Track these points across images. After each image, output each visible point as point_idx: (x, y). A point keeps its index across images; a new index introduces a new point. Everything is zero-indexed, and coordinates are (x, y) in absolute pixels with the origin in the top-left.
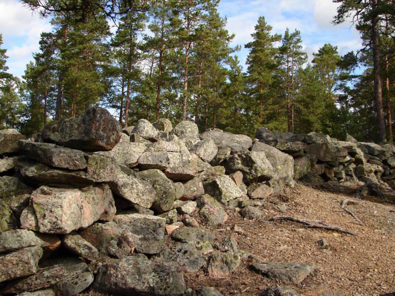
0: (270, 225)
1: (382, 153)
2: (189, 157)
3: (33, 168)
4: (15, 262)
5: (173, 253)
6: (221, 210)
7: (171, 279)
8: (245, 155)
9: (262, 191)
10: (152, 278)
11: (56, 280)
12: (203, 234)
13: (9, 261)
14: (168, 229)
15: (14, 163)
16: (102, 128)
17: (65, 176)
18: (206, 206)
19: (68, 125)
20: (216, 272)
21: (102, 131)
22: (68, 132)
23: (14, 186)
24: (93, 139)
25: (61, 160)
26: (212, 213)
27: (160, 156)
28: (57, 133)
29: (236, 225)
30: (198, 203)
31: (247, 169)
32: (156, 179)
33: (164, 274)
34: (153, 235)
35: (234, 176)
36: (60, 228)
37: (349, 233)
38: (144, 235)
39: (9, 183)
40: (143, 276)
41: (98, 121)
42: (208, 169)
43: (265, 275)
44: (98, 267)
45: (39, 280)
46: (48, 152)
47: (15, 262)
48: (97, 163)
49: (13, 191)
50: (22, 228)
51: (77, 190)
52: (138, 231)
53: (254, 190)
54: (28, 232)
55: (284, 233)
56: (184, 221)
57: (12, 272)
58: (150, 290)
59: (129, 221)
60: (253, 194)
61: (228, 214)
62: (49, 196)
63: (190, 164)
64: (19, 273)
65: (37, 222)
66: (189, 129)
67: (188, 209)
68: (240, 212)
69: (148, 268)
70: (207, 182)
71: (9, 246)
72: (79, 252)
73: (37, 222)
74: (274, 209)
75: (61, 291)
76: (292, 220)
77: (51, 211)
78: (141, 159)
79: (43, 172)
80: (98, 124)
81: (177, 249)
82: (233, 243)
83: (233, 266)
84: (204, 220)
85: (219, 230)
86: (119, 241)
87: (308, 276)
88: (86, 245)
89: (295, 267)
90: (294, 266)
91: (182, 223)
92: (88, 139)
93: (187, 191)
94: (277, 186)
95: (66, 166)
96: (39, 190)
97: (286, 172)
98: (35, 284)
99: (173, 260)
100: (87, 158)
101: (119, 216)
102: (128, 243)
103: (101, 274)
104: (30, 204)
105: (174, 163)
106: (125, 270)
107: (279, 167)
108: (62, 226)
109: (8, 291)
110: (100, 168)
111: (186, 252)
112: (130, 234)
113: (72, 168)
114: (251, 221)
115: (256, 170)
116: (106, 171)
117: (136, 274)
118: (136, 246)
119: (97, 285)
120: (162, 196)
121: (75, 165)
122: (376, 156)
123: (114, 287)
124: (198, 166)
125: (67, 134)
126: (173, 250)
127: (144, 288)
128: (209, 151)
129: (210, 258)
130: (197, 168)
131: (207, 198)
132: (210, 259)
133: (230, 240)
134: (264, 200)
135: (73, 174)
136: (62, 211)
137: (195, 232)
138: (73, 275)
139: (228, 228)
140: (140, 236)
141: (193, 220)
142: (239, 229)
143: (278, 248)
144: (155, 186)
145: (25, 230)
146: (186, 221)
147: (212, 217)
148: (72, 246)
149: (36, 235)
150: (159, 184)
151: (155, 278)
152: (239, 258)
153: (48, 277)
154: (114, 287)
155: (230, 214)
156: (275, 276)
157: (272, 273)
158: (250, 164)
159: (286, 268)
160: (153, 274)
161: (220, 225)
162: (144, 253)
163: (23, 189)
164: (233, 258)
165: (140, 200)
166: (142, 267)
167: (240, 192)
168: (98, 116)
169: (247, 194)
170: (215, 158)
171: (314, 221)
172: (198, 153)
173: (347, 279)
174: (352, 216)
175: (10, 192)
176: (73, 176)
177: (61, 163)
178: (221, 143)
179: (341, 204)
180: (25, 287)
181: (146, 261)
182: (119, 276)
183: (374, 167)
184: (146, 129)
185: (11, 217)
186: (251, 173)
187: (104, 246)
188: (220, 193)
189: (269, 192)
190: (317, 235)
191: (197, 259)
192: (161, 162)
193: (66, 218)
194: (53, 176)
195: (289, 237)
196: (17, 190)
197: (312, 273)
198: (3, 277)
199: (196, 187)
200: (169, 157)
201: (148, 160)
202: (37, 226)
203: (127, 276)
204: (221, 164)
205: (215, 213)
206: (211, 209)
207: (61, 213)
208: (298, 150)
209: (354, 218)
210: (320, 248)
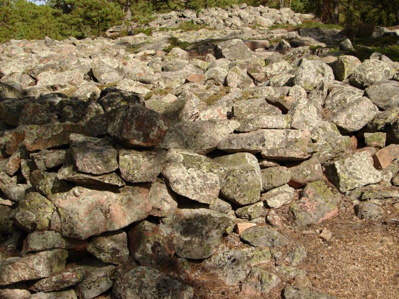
0: (379, 228)
16: (134, 127)
23: (58, 183)
27: (247, 138)
33: (165, 291)
36: (77, 235)
40: (143, 290)
41: (129, 120)
48: (129, 164)
49: (57, 189)
63: (298, 144)
66: (370, 73)
71: (33, 248)
93: (299, 174)
110: (134, 169)
113: (95, 173)
116: (141, 172)
120: (236, 189)
128: (358, 115)
130: (307, 148)
135: (97, 178)
145: (52, 232)
163: (64, 187)
164: (267, 278)
165: (198, 197)
175: (55, 189)
177: (85, 167)
178: (389, 100)
184: (304, 77)
187: (141, 248)
198: (16, 278)
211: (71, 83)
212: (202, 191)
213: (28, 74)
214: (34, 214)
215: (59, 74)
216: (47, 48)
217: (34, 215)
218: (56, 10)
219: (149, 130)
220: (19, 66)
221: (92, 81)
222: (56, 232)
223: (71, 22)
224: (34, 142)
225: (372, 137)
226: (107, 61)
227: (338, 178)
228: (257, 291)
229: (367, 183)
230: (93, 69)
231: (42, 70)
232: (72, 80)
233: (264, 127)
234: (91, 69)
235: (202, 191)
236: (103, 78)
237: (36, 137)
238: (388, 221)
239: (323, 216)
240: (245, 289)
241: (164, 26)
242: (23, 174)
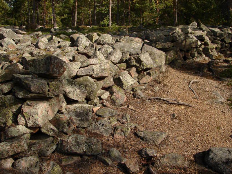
0: (148, 102)
1: (221, 35)
2: (105, 66)
3: (21, 93)
4: (17, 146)
5: (96, 125)
6: (123, 94)
7: (94, 147)
8: (137, 57)
9: (147, 79)
11: (38, 151)
12: (113, 112)
13: (14, 146)
14: (94, 110)
15: (11, 87)
17: (38, 96)
18: (115, 94)
19: (38, 64)
20: (118, 137)
22: (38, 68)
23: (12, 100)
24: (51, 74)
25: (35, 89)
26: (117, 98)
27: (88, 69)
28: (32, 67)
29: (130, 105)
30: (110, 92)
31: (138, 65)
32: (87, 83)
33: (91, 144)
34: (86, 117)
35: (130, 72)
36: (37, 125)
37: (190, 106)
38: (81, 118)
39: (10, 99)
41: (53, 64)
42: (116, 69)
43: (142, 139)
44: (58, 141)
45: (29, 153)
46: (28, 85)
47: (17, 146)
48: (54, 86)
49: (12, 103)
50: (19, 125)
51: (45, 101)
52: (78, 115)
53: (142, 78)
54: (22, 126)
55: (155, 108)
56: (102, 104)
57: (16, 150)
59: (73, 109)
60: (141, 82)
61: (127, 96)
62: (31, 108)
63: (106, 70)
64: (20, 151)
65: (26, 121)
66: (107, 39)
67: (105, 97)
68: (133, 94)
70: (115, 77)
71: (13, 135)
72: (48, 134)
73: (26, 121)
74: (152, 90)
75: (41, 153)
76: (160, 99)
77: (32, 116)
78: (78, 72)
79: (27, 95)
80: (53, 66)
81: (98, 123)
82: (127, 117)
83: (126, 133)
84: (113, 102)
85: (121, 108)
86: (68, 124)
87: (163, 140)
88: (51, 129)
89: (157, 135)
90: (157, 134)
91: (102, 105)
92: (48, 74)
93: (105, 84)
94: (154, 74)
95: (38, 92)
96: (25, 103)
97: (161, 62)
98: (28, 154)
99: (97, 129)
100: (48, 84)
101: (68, 105)
102: (73, 123)
103: (60, 144)
104: (22, 112)
105: (97, 71)
106: (71, 144)
107: (157, 60)
108: (39, 124)
109: (16, 157)
111: (103, 125)
112: (74, 117)
113: (41, 92)
114: (138, 100)
115: (143, 65)
117: (77, 145)
118: (77, 125)
119: (59, 149)
122: (217, 37)
123: (66, 152)
124: (110, 71)
125: (38, 69)
126: (96, 123)
128: (117, 57)
129: (115, 128)
130: (110, 72)
131: (116, 89)
132: (115, 129)
133: (126, 116)
134: (147, 84)
136: (38, 116)
137: (108, 111)
138: (46, 145)
139: (126, 107)
140: (79, 118)
141: (107, 104)
142: (131, 107)
143: (151, 119)
144: (87, 88)
146: (103, 104)
147: (117, 101)
148: (44, 132)
149: (26, 128)
150: (88, 87)
152: (130, 129)
153: (34, 151)
154: (66, 152)
155: (128, 96)
156: (147, 140)
157: (145, 138)
158: (140, 62)
159: (153, 135)
160: (85, 144)
161: (121, 105)
162: (82, 128)
164: (126, 129)
166: (80, 141)
167: (134, 81)
168: (53, 61)
169: (138, 82)
170: (120, 60)
171: (171, 99)
172: (110, 59)
173: (182, 142)
174: (194, 93)
175: (11, 104)
176: (42, 96)
177: (35, 90)
178: (124, 49)
179: (189, 84)
180: (23, 155)
181: (82, 137)
182: (69, 147)
183: (215, 46)
184: (82, 42)
185: (13, 116)
186: (140, 67)
187: (61, 126)
188: (123, 84)
189: (150, 80)
190: (172, 108)
192: (89, 72)
193: (40, 119)
194: (32, 97)
195: (157, 111)
197: (165, 138)
198: (12, 153)
199: (110, 81)
200: (94, 68)
202: (26, 123)
203: (73, 147)
204: (124, 62)
205: (119, 98)
206: (117, 96)
207: (37, 117)
208: (168, 47)
209: (195, 95)
210: (173, 119)
212: (80, 96)
214: (3, 118)
217: (4, 119)
219: (60, 68)
222: (22, 125)
225: (120, 65)
227: (122, 83)
228: (122, 136)
229: (131, 84)
233: (91, 64)
235: (80, 96)
238: (151, 98)
239: (124, 100)
240: (116, 136)
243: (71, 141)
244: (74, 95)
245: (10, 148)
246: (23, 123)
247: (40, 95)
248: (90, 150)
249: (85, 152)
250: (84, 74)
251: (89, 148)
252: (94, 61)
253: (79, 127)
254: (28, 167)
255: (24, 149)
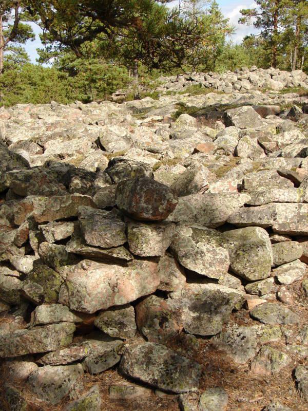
4: (31, 340)
7: (177, 375)
10: (158, 371)
12: (285, 316)
21: (145, 202)
41: (138, 194)
45: (55, 358)
54: (62, 307)
58: (154, 383)
69: (160, 358)
80: (138, 197)
105: (286, 218)
108: (85, 307)
110: (142, 242)
113: (103, 246)
120: (246, 264)
121: (106, 243)
127: (148, 379)
137: (276, 311)
145: (60, 305)
151: (162, 370)
163: (72, 259)
164: (278, 357)
165: (207, 271)
187: (148, 323)
191: (248, 348)
192: (261, 219)
196: (68, 260)
201: (242, 217)
211: (78, 152)
213: (35, 142)
214: (42, 286)
215: (67, 142)
216: (52, 113)
217: (42, 288)
218: (62, 73)
220: (26, 134)
221: (100, 150)
222: (64, 305)
223: (76, 85)
224: (43, 214)
226: (115, 130)
228: (267, 370)
230: (100, 137)
231: (49, 138)
232: (80, 149)
234: (99, 138)
236: (110, 147)
237: (45, 209)
241: (171, 89)
242: (32, 245)
243: (138, 353)
244: (196, 264)
245: (20, 341)
246: (65, 301)
247: (102, 251)
248: (167, 381)
249: (156, 381)
250: (245, 222)
251: (167, 375)
252: (286, 194)
253: (188, 333)
254: (45, 384)
255: (44, 349)
